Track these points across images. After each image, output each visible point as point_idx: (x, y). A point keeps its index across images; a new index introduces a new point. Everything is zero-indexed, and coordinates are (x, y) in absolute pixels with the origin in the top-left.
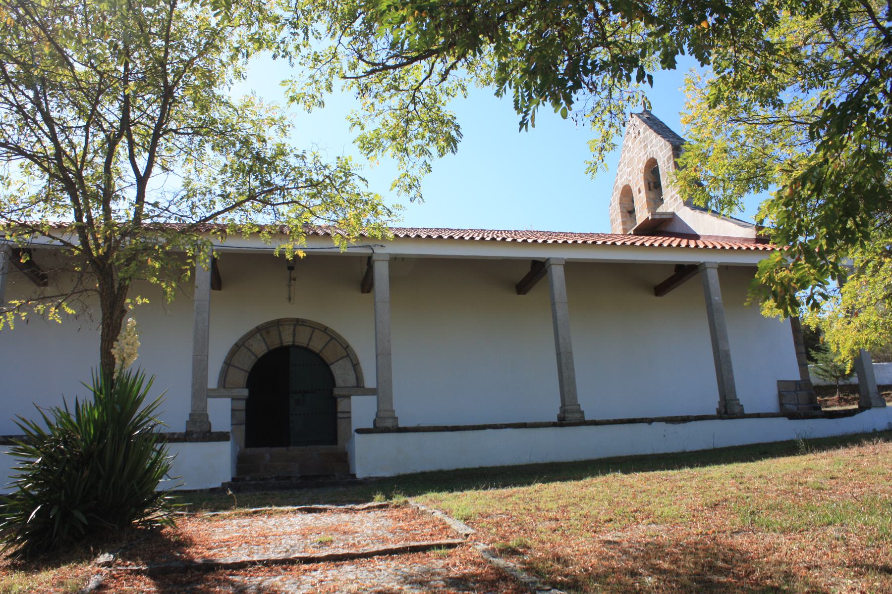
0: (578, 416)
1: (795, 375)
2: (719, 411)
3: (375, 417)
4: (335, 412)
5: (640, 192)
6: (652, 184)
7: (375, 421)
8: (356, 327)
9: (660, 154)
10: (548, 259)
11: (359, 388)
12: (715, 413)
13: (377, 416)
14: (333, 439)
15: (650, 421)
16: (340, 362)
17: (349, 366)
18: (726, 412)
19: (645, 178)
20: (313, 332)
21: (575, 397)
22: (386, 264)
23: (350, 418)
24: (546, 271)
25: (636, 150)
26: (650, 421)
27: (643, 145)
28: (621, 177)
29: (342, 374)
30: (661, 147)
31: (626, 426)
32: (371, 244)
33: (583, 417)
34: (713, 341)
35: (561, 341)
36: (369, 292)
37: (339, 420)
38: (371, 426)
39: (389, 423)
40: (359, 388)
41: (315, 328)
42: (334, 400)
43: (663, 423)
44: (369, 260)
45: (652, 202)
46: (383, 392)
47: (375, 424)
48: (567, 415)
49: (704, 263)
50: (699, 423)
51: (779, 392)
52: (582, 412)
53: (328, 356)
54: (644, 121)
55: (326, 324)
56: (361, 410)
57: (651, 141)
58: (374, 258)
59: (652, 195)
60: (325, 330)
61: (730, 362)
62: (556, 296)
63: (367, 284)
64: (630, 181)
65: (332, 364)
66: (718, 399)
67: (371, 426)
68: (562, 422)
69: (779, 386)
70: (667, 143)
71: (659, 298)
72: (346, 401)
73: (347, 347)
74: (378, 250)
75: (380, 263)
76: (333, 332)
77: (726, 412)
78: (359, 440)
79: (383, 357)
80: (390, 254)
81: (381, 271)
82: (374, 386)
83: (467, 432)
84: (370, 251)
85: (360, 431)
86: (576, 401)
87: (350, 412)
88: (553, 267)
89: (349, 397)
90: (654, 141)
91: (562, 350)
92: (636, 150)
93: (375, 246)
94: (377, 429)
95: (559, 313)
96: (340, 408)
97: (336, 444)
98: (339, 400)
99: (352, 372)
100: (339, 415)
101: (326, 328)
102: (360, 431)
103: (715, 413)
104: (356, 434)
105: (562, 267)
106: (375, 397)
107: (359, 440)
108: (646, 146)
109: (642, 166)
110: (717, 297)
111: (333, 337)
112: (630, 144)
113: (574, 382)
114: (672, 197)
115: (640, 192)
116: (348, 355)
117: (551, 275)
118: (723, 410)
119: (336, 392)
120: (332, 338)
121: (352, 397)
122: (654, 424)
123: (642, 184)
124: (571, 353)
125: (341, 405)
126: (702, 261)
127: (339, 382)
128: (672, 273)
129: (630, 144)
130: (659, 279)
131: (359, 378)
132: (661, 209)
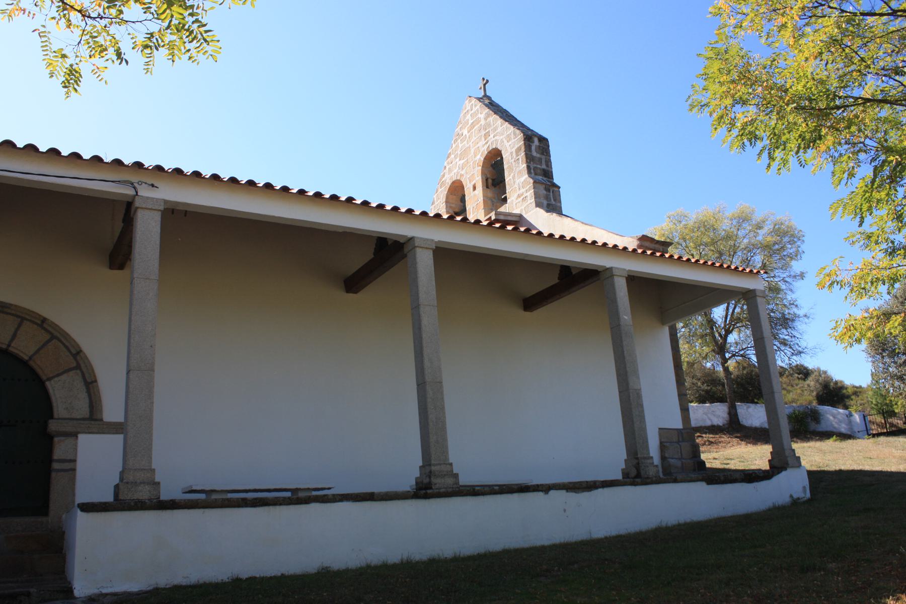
0: (450, 481)
1: (677, 423)
2: (626, 474)
3: (117, 481)
4: (48, 459)
5: (474, 188)
6: (490, 181)
7: (117, 487)
8: (96, 321)
9: (507, 144)
10: (412, 239)
11: (93, 421)
12: (619, 476)
13: (121, 479)
14: (42, 506)
15: (546, 489)
16: (64, 377)
17: (79, 384)
18: (638, 475)
19: (483, 173)
20: (20, 325)
21: (445, 452)
22: (157, 217)
23: (74, 470)
24: (405, 256)
25: (474, 139)
26: (546, 489)
27: (483, 133)
28: (450, 170)
29: (65, 396)
30: (508, 136)
31: (516, 497)
32: (134, 178)
33: (457, 483)
34: (618, 375)
35: (427, 363)
36: (121, 267)
37: (53, 474)
38: (110, 498)
39: (143, 493)
40: (93, 421)
41: (23, 319)
42: (48, 440)
43: (563, 493)
44: (127, 210)
45: (489, 202)
46: (134, 431)
47: (116, 494)
48: (434, 480)
49: (611, 269)
50: (607, 491)
51: (661, 443)
52: (456, 476)
53: (42, 365)
54: (486, 105)
55: (45, 313)
56: (95, 462)
57: (495, 129)
58: (137, 203)
59: (490, 194)
60: (42, 323)
61: (642, 406)
62: (422, 296)
63: (120, 255)
64: (462, 175)
65: (49, 379)
66: (624, 456)
67: (110, 498)
68: (423, 490)
69: (660, 435)
70: (518, 132)
71: (528, 313)
72: (69, 441)
73: (78, 354)
74: (144, 192)
75: (147, 212)
76: (55, 326)
77: (638, 475)
78: (84, 523)
79: (140, 374)
80: (166, 202)
81: (148, 230)
82: (121, 419)
83: (278, 509)
84: (130, 192)
85: (87, 508)
86: (447, 458)
87: (75, 461)
88: (418, 250)
89: (75, 435)
90: (500, 129)
91: (428, 378)
92: (474, 139)
93: (140, 183)
94: (120, 503)
95: (425, 321)
96: (58, 453)
97: (46, 514)
98: (56, 439)
99: (83, 395)
100: (56, 466)
101: (44, 320)
102: (87, 508)
103: (619, 476)
104: (79, 512)
105: (431, 253)
106: (121, 436)
107: (84, 523)
108: (487, 135)
109: (480, 158)
110: (626, 316)
111: (54, 335)
112: (465, 132)
113: (444, 429)
114: (519, 196)
115: (474, 188)
116: (78, 367)
117: (415, 263)
118: (633, 472)
119: (53, 426)
120: (53, 337)
121: (80, 436)
122: (552, 492)
123: (478, 180)
124: (441, 383)
125: (60, 450)
126: (608, 265)
127: (60, 410)
128: (553, 280)
129: (465, 132)
130: (531, 288)
131: (94, 404)
132: (504, 209)
